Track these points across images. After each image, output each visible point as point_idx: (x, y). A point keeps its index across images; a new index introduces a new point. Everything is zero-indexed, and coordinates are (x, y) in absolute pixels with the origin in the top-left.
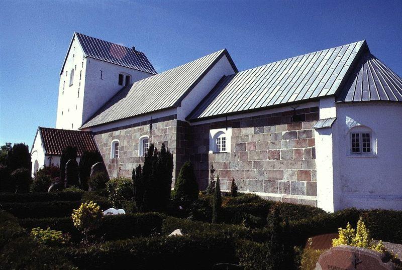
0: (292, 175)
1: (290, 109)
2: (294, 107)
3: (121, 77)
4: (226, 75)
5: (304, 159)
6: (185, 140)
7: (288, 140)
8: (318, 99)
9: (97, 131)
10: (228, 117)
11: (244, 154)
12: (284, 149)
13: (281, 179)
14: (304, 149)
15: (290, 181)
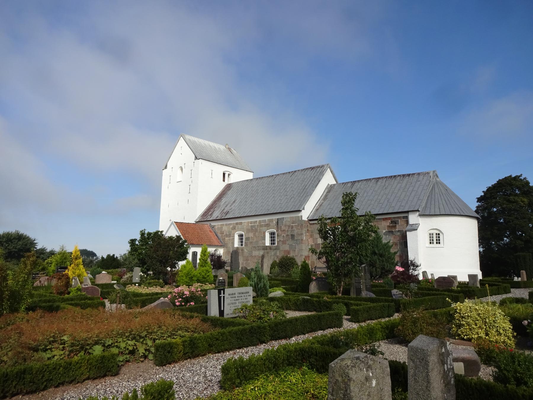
8: (407, 212)
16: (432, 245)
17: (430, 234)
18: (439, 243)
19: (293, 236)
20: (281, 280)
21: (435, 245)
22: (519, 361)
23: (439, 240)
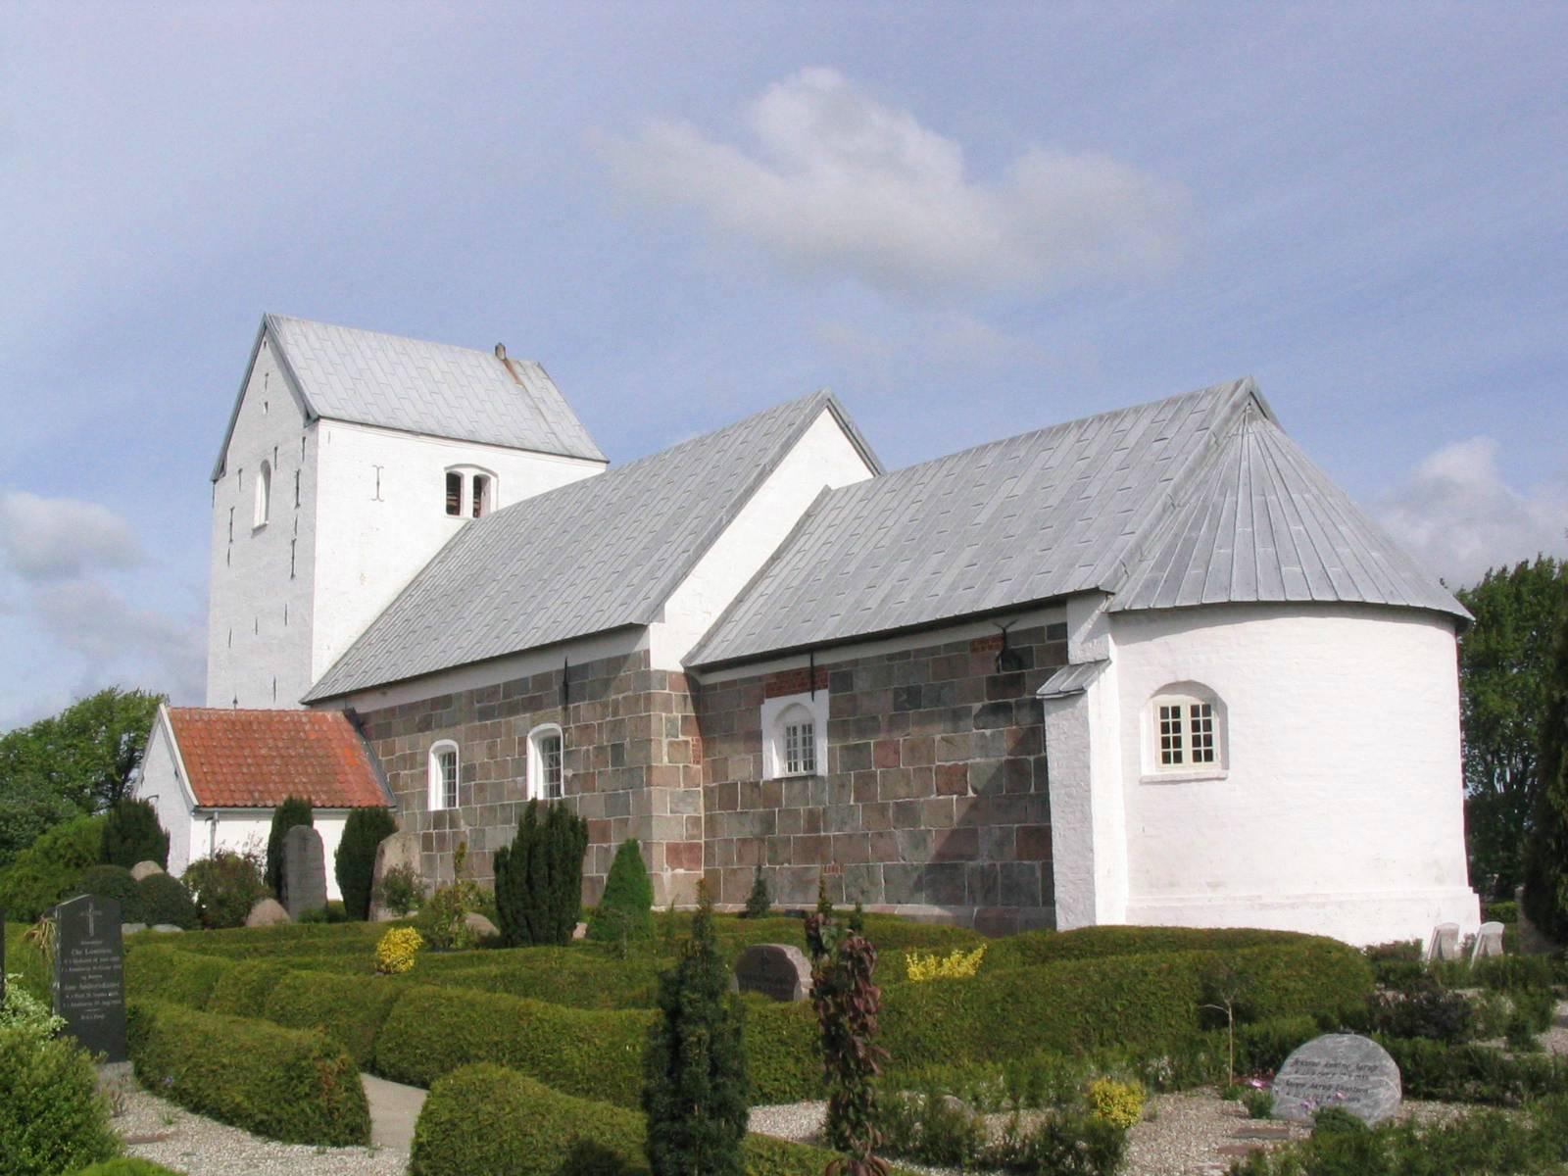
0: (1001, 844)
1: (991, 630)
2: (1004, 622)
3: (454, 482)
4: (833, 488)
5: (1032, 790)
6: (681, 738)
7: (988, 732)
8: (1058, 602)
9: (602, 1105)
10: (816, 655)
11: (865, 781)
12: (978, 760)
13: (972, 858)
14: (1032, 758)
15: (998, 864)
16: (1173, 770)
17: (1164, 711)
18: (1209, 756)
19: (617, 750)
20: (103, 973)
21: (1188, 767)
22: (590, 1026)
23: (1209, 741)
